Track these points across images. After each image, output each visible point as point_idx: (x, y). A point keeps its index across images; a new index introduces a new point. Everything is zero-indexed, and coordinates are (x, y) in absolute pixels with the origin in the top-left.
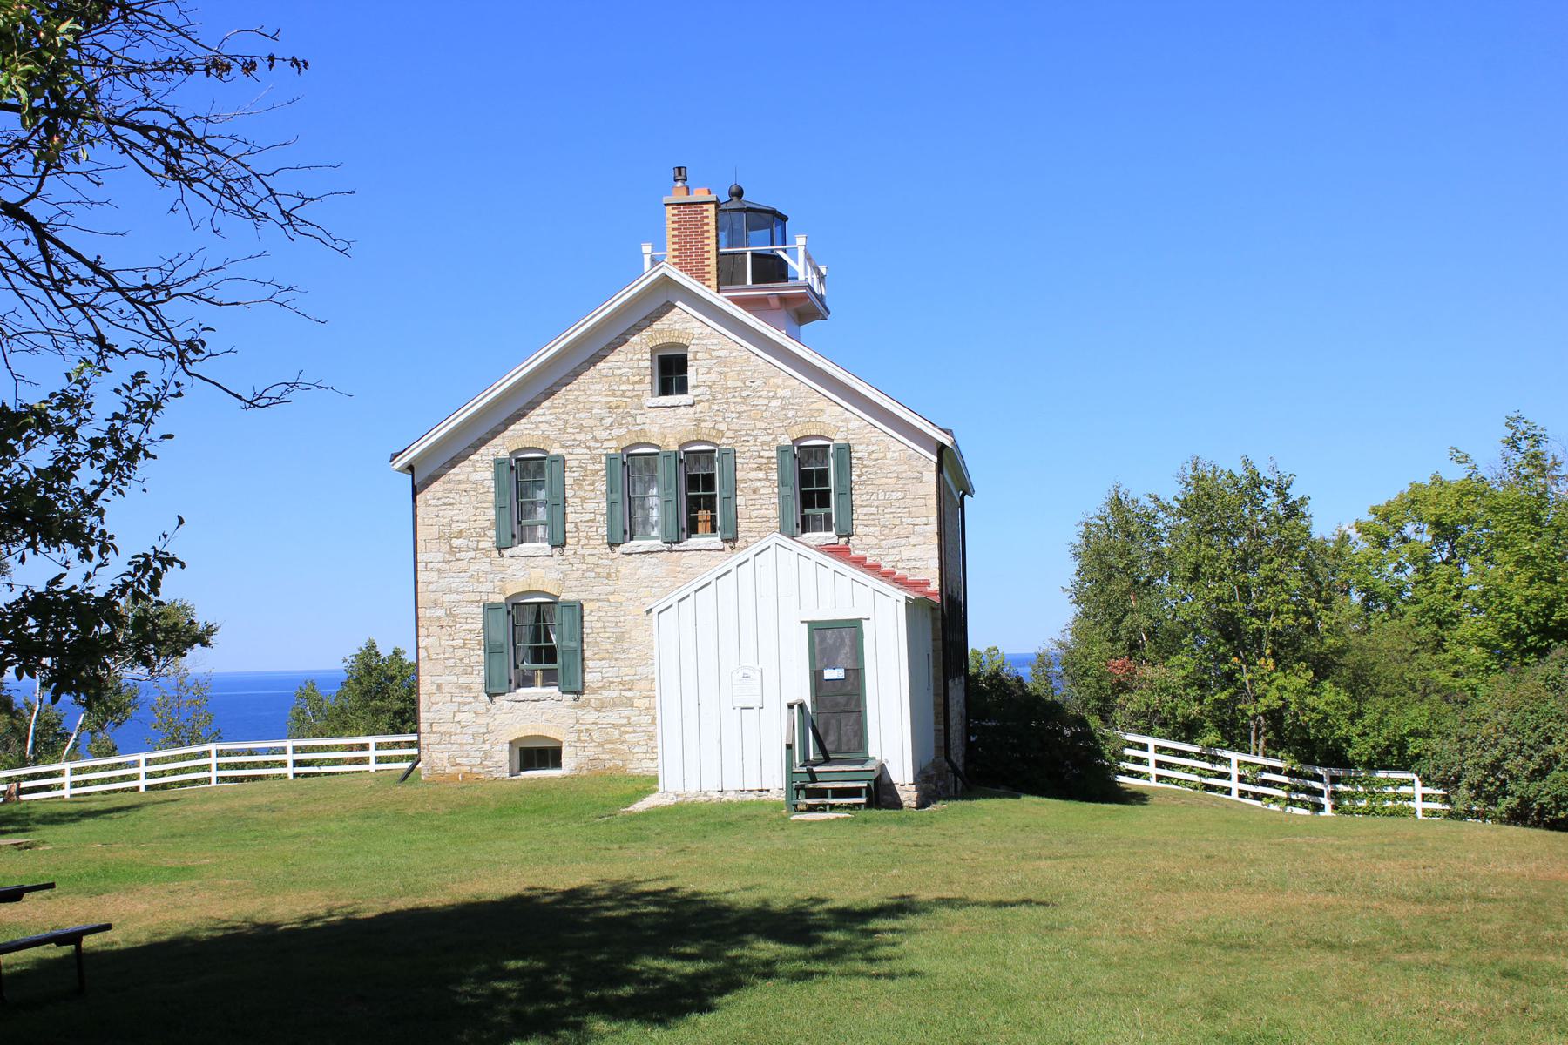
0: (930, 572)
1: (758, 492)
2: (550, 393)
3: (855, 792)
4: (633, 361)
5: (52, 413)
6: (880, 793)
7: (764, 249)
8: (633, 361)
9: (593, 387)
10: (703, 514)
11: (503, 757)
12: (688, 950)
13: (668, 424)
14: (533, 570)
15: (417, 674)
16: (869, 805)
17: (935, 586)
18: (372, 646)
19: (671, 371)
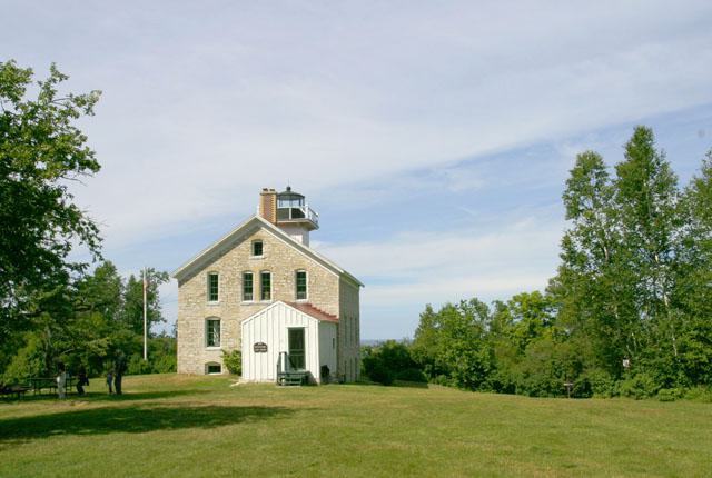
0: (333, 308)
1: (283, 285)
2: (221, 255)
3: (298, 380)
4: (247, 245)
5: (679, 230)
6: (307, 380)
7: (297, 207)
8: (247, 245)
9: (234, 253)
10: (267, 293)
11: (203, 368)
12: (337, 421)
13: (256, 265)
14: (213, 309)
15: (176, 345)
16: (302, 384)
17: (338, 317)
18: (429, 309)
19: (258, 249)
